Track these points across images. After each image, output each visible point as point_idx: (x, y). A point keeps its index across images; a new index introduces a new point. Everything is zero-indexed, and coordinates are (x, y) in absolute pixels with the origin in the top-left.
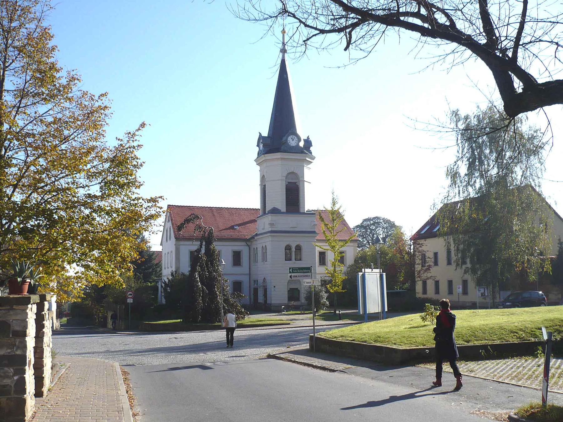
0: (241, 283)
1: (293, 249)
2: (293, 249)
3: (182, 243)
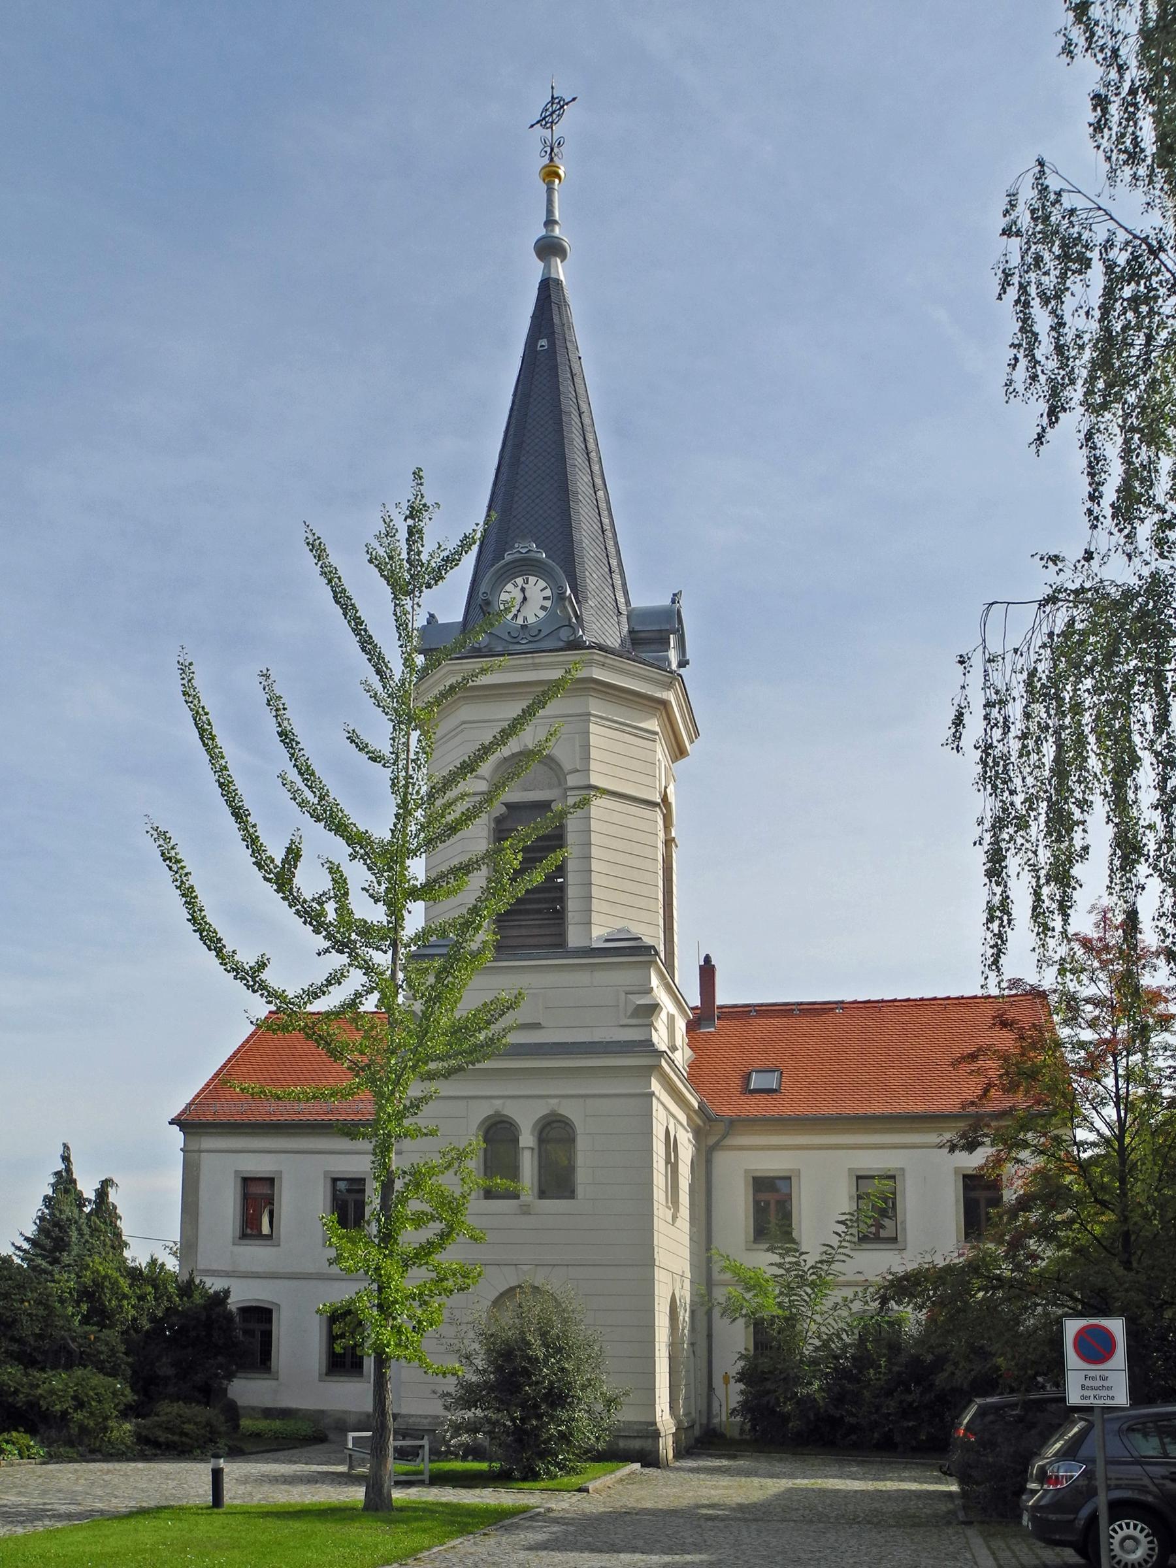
0: (270, 1311)
1: (527, 1139)
2: (527, 1139)
3: (208, 1143)
